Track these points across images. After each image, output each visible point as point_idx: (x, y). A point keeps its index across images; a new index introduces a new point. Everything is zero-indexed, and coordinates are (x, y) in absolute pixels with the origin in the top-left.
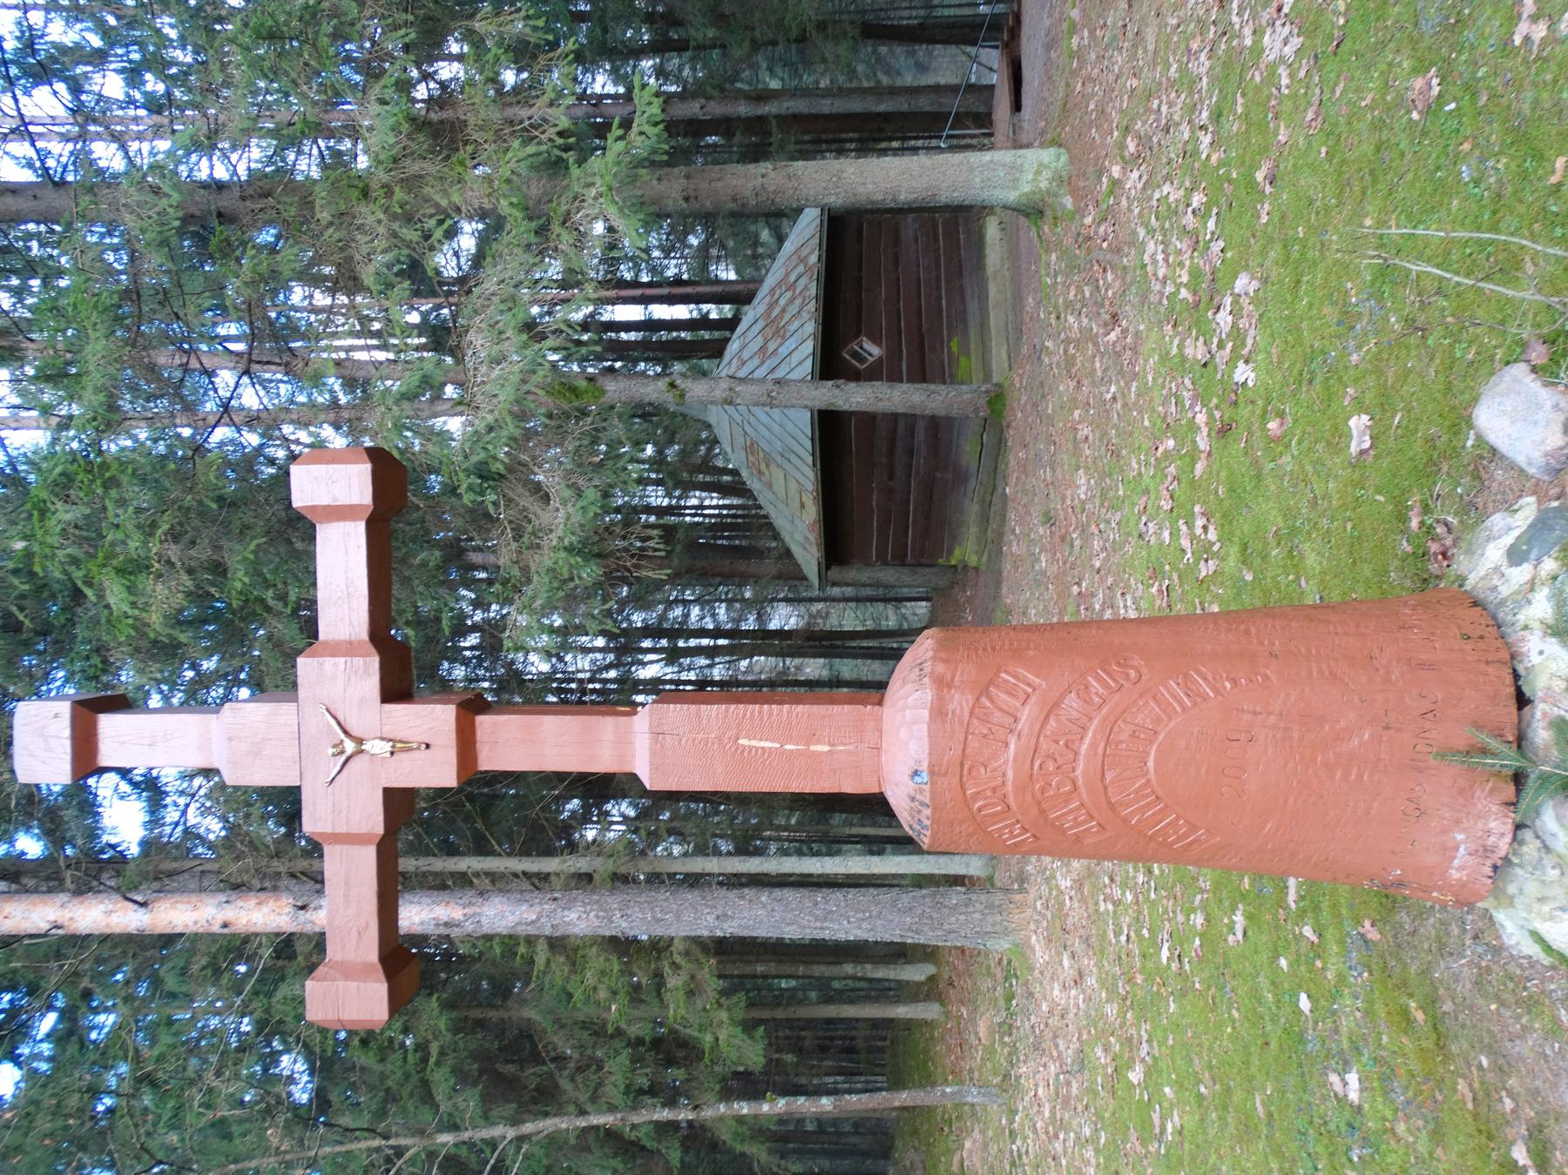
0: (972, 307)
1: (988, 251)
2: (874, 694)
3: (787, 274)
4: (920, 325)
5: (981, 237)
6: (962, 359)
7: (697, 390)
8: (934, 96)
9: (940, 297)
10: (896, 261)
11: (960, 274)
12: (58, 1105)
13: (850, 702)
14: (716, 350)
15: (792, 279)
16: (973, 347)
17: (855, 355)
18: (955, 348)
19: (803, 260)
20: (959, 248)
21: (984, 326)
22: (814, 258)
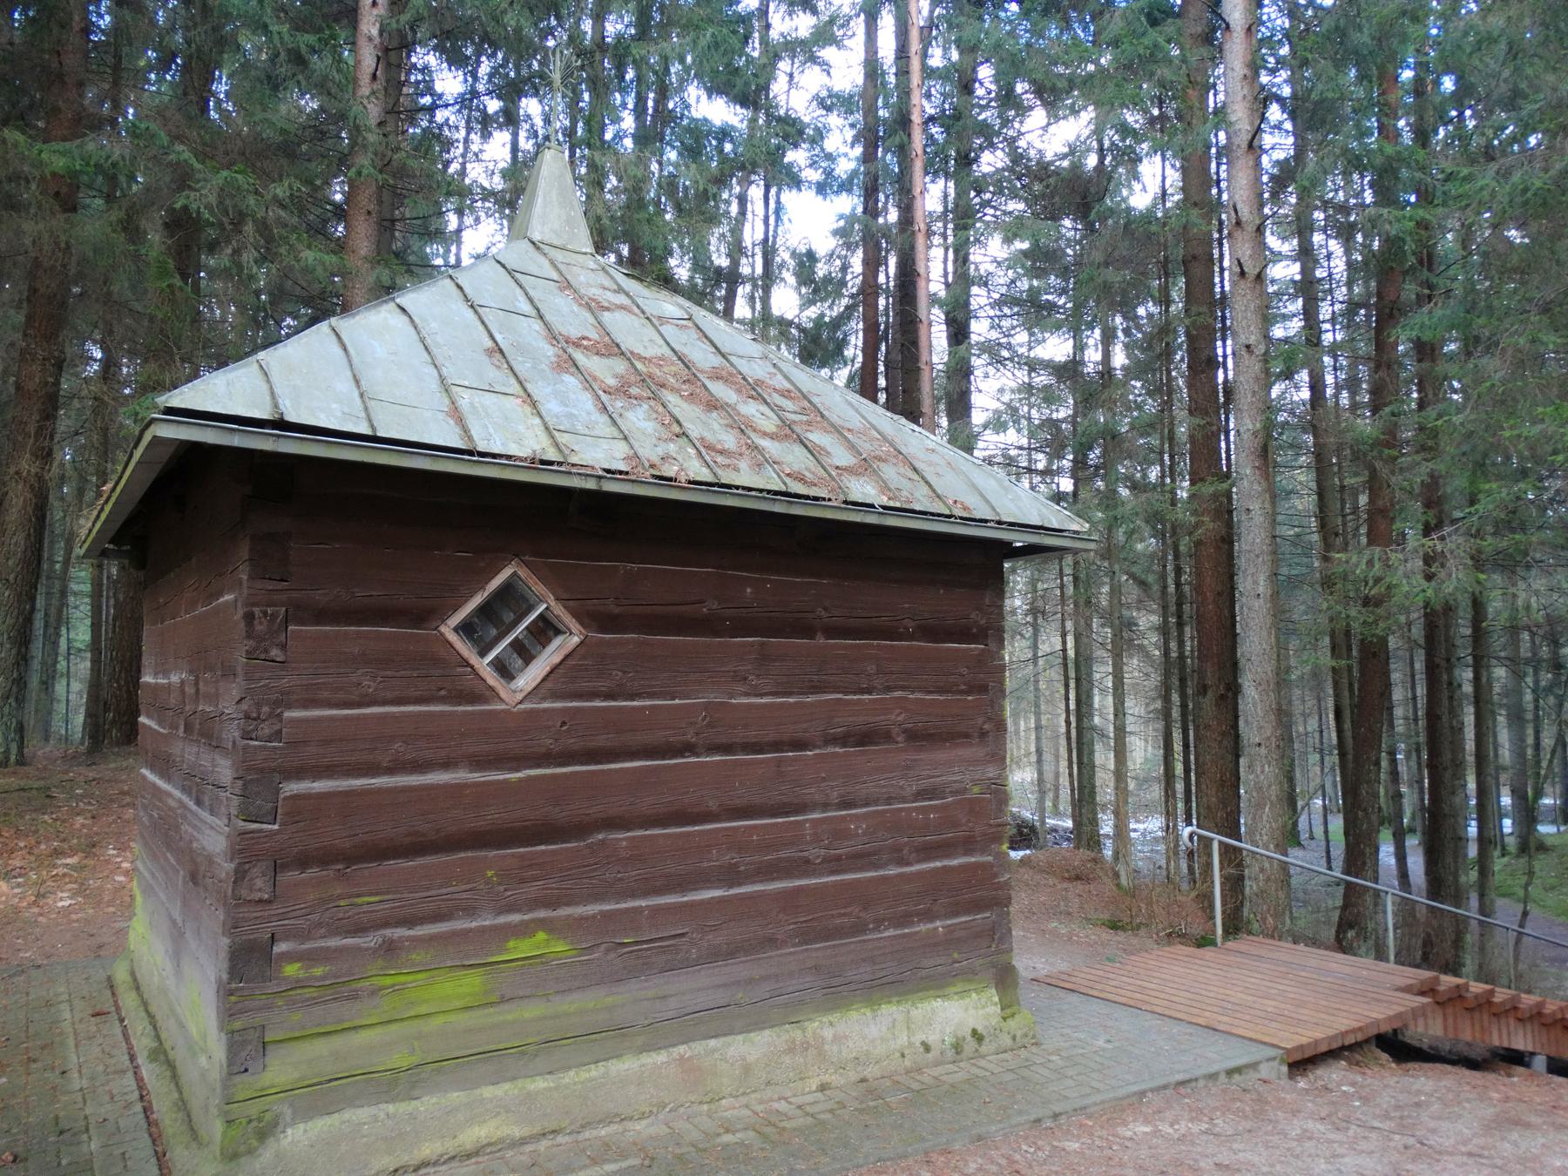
0: (692, 987)
1: (890, 1011)
2: (1298, 1057)
3: (837, 430)
4: (611, 824)
5: (937, 983)
6: (471, 983)
7: (843, 374)
8: (1274, 791)
9: (731, 876)
10: (865, 738)
11: (807, 935)
12: (829, 173)
13: (1344, 1034)
14: (906, 405)
15: (816, 437)
16: (530, 1011)
17: (510, 600)
18: (520, 948)
19: (866, 466)
20: (903, 920)
21: (613, 1036)
22: (863, 489)
